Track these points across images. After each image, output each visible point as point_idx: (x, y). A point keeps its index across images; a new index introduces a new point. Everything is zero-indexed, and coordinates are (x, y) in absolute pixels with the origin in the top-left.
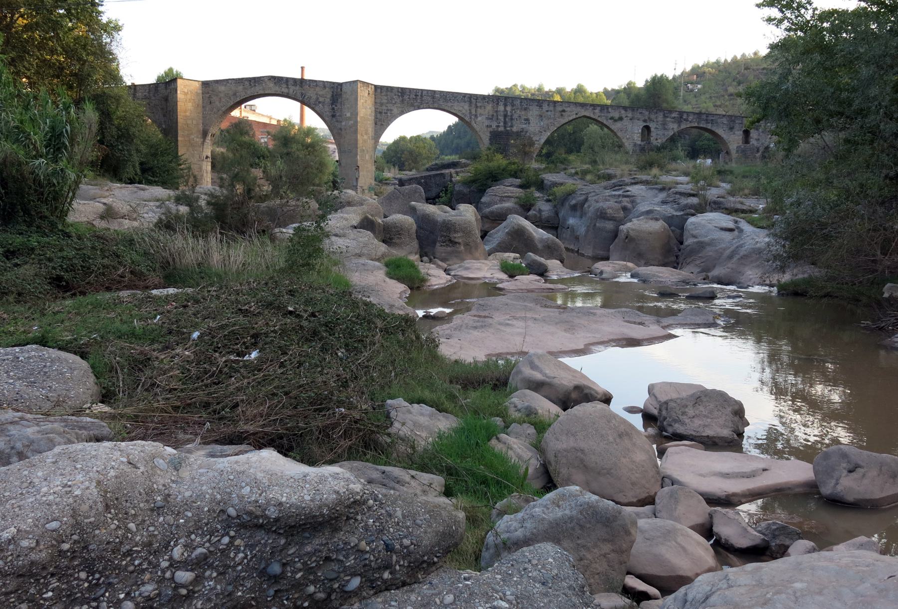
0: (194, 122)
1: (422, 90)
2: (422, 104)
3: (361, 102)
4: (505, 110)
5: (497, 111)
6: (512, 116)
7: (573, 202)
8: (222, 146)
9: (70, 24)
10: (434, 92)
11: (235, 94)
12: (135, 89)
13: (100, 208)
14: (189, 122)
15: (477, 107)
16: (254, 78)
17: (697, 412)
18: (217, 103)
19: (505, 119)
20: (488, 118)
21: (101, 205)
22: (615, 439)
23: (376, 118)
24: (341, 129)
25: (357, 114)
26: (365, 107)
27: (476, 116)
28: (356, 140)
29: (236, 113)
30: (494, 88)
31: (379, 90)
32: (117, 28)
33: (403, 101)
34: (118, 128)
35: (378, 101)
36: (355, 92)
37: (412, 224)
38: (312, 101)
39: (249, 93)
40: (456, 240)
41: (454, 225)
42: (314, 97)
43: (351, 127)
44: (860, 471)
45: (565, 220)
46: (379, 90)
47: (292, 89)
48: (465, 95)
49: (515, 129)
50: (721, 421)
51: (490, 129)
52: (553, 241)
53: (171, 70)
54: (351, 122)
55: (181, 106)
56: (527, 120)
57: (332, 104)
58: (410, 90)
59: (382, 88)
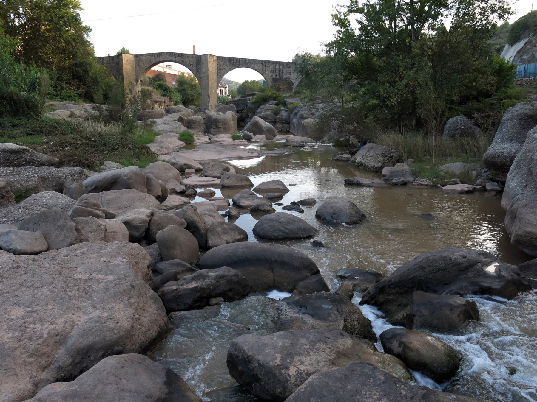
1: (240, 59)
3: (210, 64)
7: (296, 111)
9: (66, 29)
10: (245, 59)
11: (150, 61)
14: (129, 75)
16: (159, 53)
20: (271, 72)
23: (218, 72)
26: (212, 67)
29: (155, 68)
32: (90, 30)
33: (230, 64)
38: (187, 64)
39: (157, 60)
41: (218, 120)
42: (188, 62)
45: (292, 120)
47: (177, 58)
48: (260, 61)
49: (284, 77)
52: (271, 127)
53: (124, 48)
55: (124, 67)
58: (234, 58)
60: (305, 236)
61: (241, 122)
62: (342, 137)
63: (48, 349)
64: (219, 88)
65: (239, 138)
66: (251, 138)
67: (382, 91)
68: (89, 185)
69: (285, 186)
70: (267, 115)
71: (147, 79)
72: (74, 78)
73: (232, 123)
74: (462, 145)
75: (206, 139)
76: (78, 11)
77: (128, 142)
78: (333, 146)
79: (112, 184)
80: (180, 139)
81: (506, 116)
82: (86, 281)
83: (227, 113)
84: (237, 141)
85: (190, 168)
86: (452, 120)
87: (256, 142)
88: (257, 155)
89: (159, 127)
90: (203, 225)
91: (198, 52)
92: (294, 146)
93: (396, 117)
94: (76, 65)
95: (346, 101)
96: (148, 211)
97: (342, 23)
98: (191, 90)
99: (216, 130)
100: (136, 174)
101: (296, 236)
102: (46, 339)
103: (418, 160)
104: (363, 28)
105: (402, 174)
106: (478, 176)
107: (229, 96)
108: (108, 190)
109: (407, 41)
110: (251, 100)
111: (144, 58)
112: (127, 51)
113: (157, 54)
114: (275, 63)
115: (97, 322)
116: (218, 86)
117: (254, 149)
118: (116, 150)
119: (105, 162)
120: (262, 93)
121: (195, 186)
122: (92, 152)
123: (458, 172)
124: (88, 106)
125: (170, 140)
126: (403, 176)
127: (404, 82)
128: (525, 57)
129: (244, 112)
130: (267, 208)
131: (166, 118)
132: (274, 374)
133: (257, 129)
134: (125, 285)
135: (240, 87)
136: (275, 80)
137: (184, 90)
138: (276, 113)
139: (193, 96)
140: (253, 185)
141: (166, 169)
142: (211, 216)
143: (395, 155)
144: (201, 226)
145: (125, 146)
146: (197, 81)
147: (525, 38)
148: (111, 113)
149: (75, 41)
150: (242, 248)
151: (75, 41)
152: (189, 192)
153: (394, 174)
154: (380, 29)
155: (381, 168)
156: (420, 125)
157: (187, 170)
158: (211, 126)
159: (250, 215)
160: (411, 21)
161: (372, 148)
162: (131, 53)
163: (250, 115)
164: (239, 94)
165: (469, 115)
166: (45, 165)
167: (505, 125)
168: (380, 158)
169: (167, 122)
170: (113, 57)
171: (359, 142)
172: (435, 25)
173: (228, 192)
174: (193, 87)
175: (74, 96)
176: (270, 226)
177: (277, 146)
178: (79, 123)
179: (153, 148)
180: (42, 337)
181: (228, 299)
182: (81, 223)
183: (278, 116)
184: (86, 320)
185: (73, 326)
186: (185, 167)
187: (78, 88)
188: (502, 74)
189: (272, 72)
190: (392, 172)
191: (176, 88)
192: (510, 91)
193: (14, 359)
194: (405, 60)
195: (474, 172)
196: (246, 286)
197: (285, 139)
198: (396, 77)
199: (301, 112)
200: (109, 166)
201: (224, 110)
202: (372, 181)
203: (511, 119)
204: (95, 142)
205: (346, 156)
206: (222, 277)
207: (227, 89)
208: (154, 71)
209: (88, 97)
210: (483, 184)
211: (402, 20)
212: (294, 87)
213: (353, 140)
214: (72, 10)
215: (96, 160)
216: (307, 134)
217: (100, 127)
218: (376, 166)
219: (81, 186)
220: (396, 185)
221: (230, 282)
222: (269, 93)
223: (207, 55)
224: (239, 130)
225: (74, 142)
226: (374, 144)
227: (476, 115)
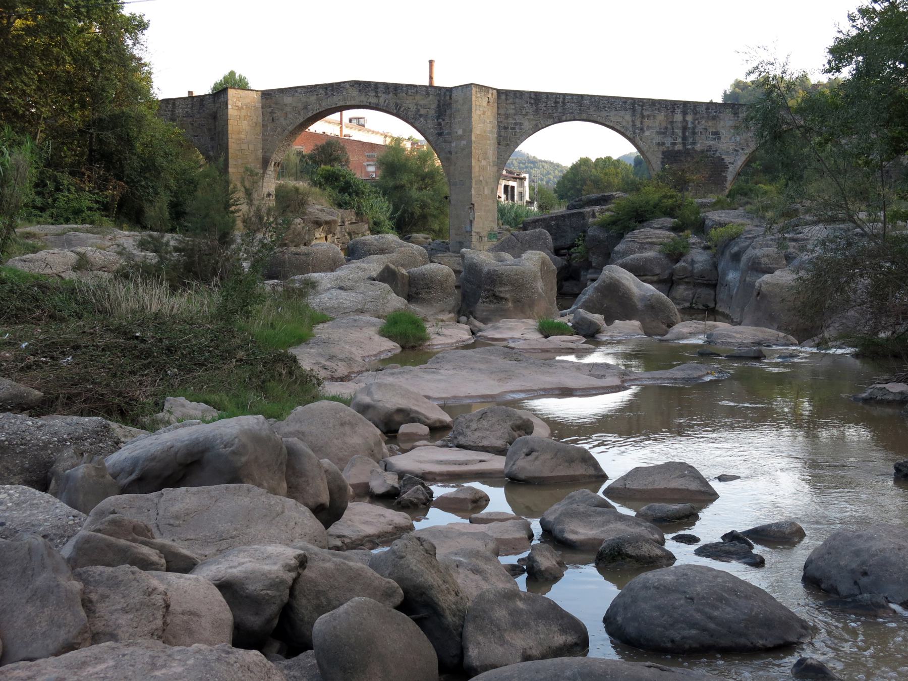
0: (251, 147)
1: (565, 95)
2: (564, 114)
4: (684, 120)
5: (672, 122)
6: (694, 128)
7: (736, 249)
9: (80, 25)
10: (582, 96)
11: (306, 108)
12: (174, 104)
14: (244, 147)
15: (643, 117)
16: (332, 85)
17: (480, 426)
18: (282, 119)
19: (684, 133)
21: (73, 255)
22: (334, 426)
23: (499, 135)
24: (450, 152)
25: (471, 131)
26: (483, 121)
27: (642, 130)
28: (470, 167)
29: (318, 127)
30: (732, 82)
31: (503, 97)
32: (142, 26)
33: (537, 111)
35: (502, 112)
36: (468, 101)
37: (449, 275)
38: (411, 114)
39: (326, 105)
40: (502, 295)
42: (413, 108)
43: (463, 150)
44: (534, 454)
45: (725, 274)
46: (503, 97)
47: (383, 97)
48: (625, 100)
49: (698, 147)
50: (499, 434)
51: (662, 148)
53: (232, 74)
54: (464, 142)
56: (716, 133)
57: (438, 117)
58: (548, 95)
59: (507, 92)
60: (769, 643)
61: (569, 281)
64: (503, 183)
65: (560, 330)
66: (598, 331)
69: (704, 482)
71: (295, 159)
72: (91, 160)
73: (540, 285)
75: (461, 333)
78: (856, 356)
79: (186, 468)
80: (385, 333)
83: (524, 256)
85: (413, 420)
88: (616, 381)
89: (325, 297)
90: (452, 598)
92: (733, 357)
94: (99, 123)
96: (290, 553)
98: (420, 189)
99: (492, 306)
101: (743, 641)
107: (530, 203)
110: (599, 218)
116: (499, 177)
117: (607, 366)
118: (201, 365)
119: (171, 402)
121: (426, 478)
122: (132, 372)
124: (128, 238)
125: (355, 335)
130: (647, 550)
131: (349, 271)
133: (617, 304)
136: (670, 156)
137: (399, 188)
139: (424, 206)
140: (604, 477)
142: (476, 571)
145: (229, 354)
146: (438, 163)
148: (190, 257)
149: (100, 58)
151: (100, 58)
152: (408, 495)
157: (404, 429)
158: (478, 295)
162: (253, 85)
163: (595, 260)
164: (561, 197)
169: (349, 284)
170: (202, 98)
173: (528, 496)
174: (427, 179)
175: (90, 209)
176: (659, 608)
178: (99, 286)
179: (307, 359)
182: (98, 583)
183: (681, 264)
186: (397, 418)
187: (102, 185)
189: (663, 133)
191: (375, 184)
197: (703, 333)
199: (750, 252)
200: (178, 412)
204: (143, 341)
207: (526, 183)
208: (315, 135)
209: (128, 212)
215: (143, 395)
216: (767, 318)
217: (158, 300)
219: (101, 470)
222: (652, 194)
224: (562, 307)
225: (84, 341)
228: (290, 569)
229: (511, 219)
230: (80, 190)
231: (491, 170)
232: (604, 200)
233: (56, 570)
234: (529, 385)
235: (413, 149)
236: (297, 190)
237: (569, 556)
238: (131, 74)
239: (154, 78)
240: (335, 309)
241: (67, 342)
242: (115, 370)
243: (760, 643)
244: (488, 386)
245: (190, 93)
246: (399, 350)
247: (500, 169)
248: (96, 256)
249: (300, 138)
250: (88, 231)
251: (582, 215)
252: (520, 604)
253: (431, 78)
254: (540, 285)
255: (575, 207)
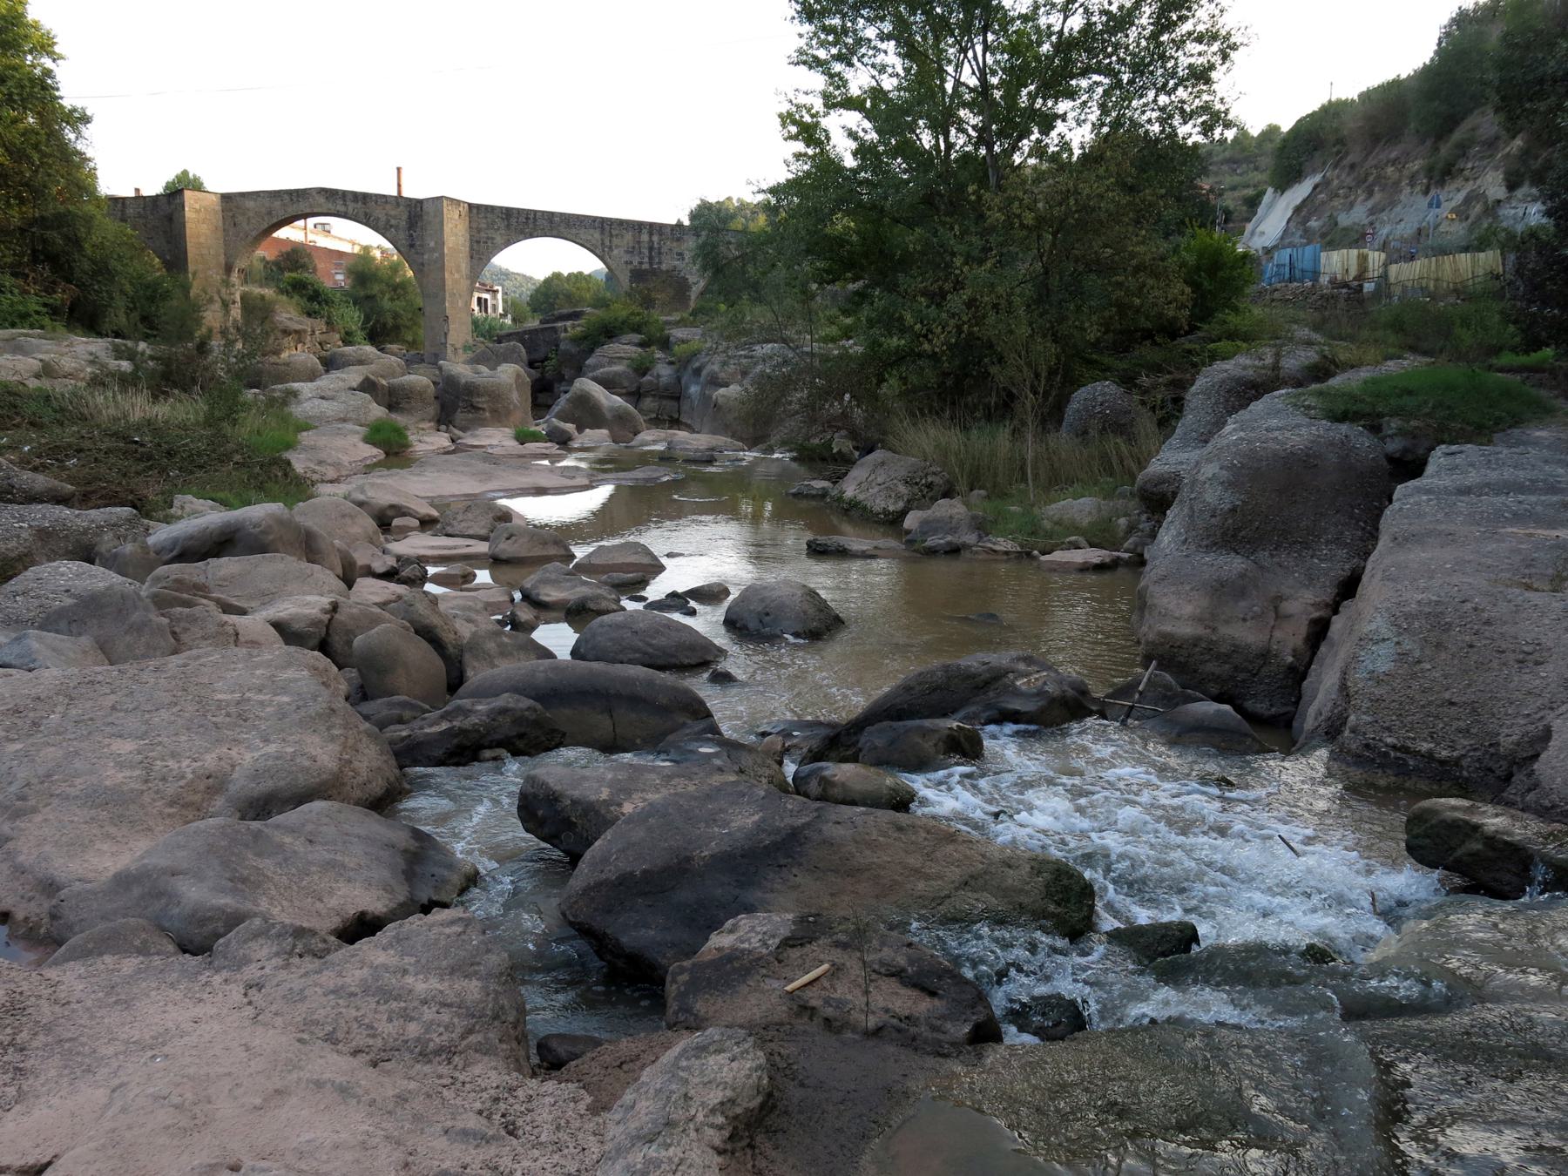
3: (447, 228)
7: (697, 364)
8: (267, 286)
11: (269, 213)
13: (34, 364)
14: (205, 252)
18: (244, 225)
23: (472, 249)
26: (455, 234)
28: (443, 280)
29: (283, 233)
32: (85, 119)
33: (508, 227)
34: (94, 262)
35: (474, 225)
36: (439, 214)
38: (381, 224)
39: (291, 211)
42: (383, 219)
45: (687, 388)
47: (351, 206)
48: (595, 219)
49: (664, 267)
52: (628, 413)
53: (185, 173)
56: (680, 254)
58: (519, 211)
59: (479, 207)
60: (693, 661)
61: (543, 393)
62: (815, 435)
63: (197, 798)
64: (476, 295)
65: (535, 437)
66: (570, 439)
67: (908, 317)
68: (163, 548)
69: (655, 558)
70: (616, 373)
71: (259, 266)
72: (35, 260)
73: (515, 396)
74: (1105, 457)
75: (442, 440)
76: (47, 62)
77: (230, 446)
78: (794, 459)
79: (223, 543)
80: (368, 440)
81: (1201, 382)
82: (238, 703)
83: (499, 369)
84: (532, 447)
85: (404, 515)
86: (1081, 394)
87: (583, 449)
88: (586, 482)
89: (307, 406)
90: (452, 636)
91: (410, 192)
92: (687, 461)
93: (949, 383)
94: (42, 222)
95: (827, 334)
96: (325, 601)
97: (809, 133)
98: (392, 299)
100: (280, 522)
101: (673, 660)
102: (192, 781)
103: (998, 493)
104: (863, 151)
105: (950, 526)
106: (1131, 529)
107: (504, 316)
108: (217, 555)
109: (971, 189)
110: (571, 332)
111: (250, 204)
112: (196, 179)
113: (290, 193)
114: (638, 227)
115: (278, 758)
116: (472, 290)
117: (577, 468)
118: (201, 467)
119: (179, 499)
120: (600, 313)
121: (422, 560)
122: (138, 473)
123: (1085, 522)
124: (98, 346)
125: (339, 442)
126: (953, 530)
127: (966, 295)
128: (1314, 224)
129: (550, 365)
130: (604, 605)
131: (328, 382)
132: (597, 813)
133: (586, 414)
134: (321, 705)
135: (537, 290)
136: (638, 275)
137: (370, 298)
138: (642, 369)
139: (396, 316)
140: (573, 557)
141: (344, 516)
142: (469, 621)
143: (937, 480)
144: (448, 638)
145: (225, 458)
146: (410, 273)
147: (1314, 171)
148: (167, 366)
149: (40, 151)
150: (545, 671)
151: (40, 151)
152: (406, 572)
153: (928, 527)
154: (908, 150)
155: (903, 514)
156: (1004, 408)
157: (396, 522)
158: (456, 406)
159: (566, 625)
160: (984, 137)
161: (883, 463)
162: (209, 186)
163: (567, 373)
164: (534, 310)
165: (1128, 381)
166: (42, 502)
167: (1192, 405)
168: (902, 489)
169: (330, 394)
170: (155, 199)
171: (856, 448)
172: (1047, 145)
173: (509, 573)
174: (399, 289)
175: (38, 313)
176: (611, 639)
177: (645, 459)
178: (74, 394)
179: (299, 463)
180: (183, 777)
181: (516, 753)
182: (179, 620)
183: (647, 378)
184: (251, 758)
185: (233, 766)
186: (390, 513)
187: (50, 289)
188: (1221, 274)
189: (630, 252)
190: (924, 523)
191: (346, 294)
192: (1233, 320)
193: (142, 806)
194: (967, 238)
195: (1123, 521)
196: (554, 731)
197: (664, 440)
198: (946, 280)
199: (709, 368)
200: (188, 508)
201: (491, 360)
202: (875, 543)
203: (1206, 392)
204: (142, 445)
205: (819, 484)
206: (504, 711)
207: (500, 296)
208: (278, 240)
209: (84, 317)
210: (1139, 550)
211: (964, 131)
212: (694, 293)
213: (841, 444)
214: (29, 57)
215: (152, 493)
216: (725, 429)
217: (138, 407)
218: (891, 508)
219: (145, 547)
220: (932, 552)
221: (519, 720)
222: (620, 311)
223: (440, 198)
224: (537, 417)
225: (87, 444)
226: (889, 454)
227: (1144, 380)
228: (326, 612)
229: (484, 331)
230: (24, 292)
231: (465, 283)
232: (575, 316)
233: (146, 609)
234: (507, 485)
235: (384, 259)
236: (263, 297)
237: (544, 615)
238: (74, 167)
239: (98, 173)
240: (320, 418)
241: (70, 446)
242: (133, 472)
243: (686, 661)
244: (470, 486)
245: (137, 190)
246: (383, 456)
247: (473, 283)
248: (67, 364)
249: (265, 243)
250: (40, 337)
251: (554, 330)
252: (506, 640)
253: (399, 191)
254: (515, 396)
255: (548, 322)
